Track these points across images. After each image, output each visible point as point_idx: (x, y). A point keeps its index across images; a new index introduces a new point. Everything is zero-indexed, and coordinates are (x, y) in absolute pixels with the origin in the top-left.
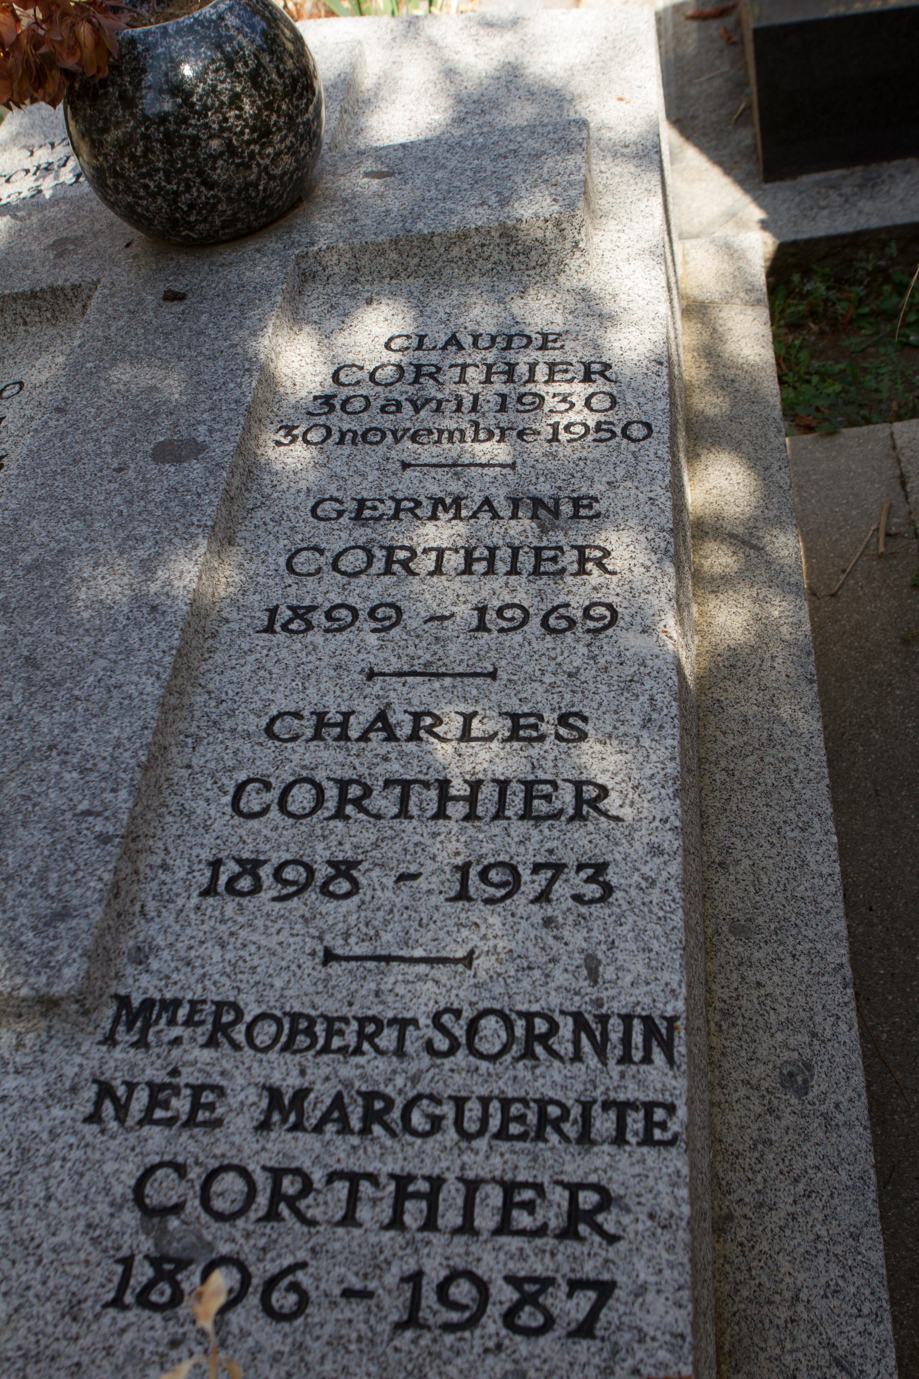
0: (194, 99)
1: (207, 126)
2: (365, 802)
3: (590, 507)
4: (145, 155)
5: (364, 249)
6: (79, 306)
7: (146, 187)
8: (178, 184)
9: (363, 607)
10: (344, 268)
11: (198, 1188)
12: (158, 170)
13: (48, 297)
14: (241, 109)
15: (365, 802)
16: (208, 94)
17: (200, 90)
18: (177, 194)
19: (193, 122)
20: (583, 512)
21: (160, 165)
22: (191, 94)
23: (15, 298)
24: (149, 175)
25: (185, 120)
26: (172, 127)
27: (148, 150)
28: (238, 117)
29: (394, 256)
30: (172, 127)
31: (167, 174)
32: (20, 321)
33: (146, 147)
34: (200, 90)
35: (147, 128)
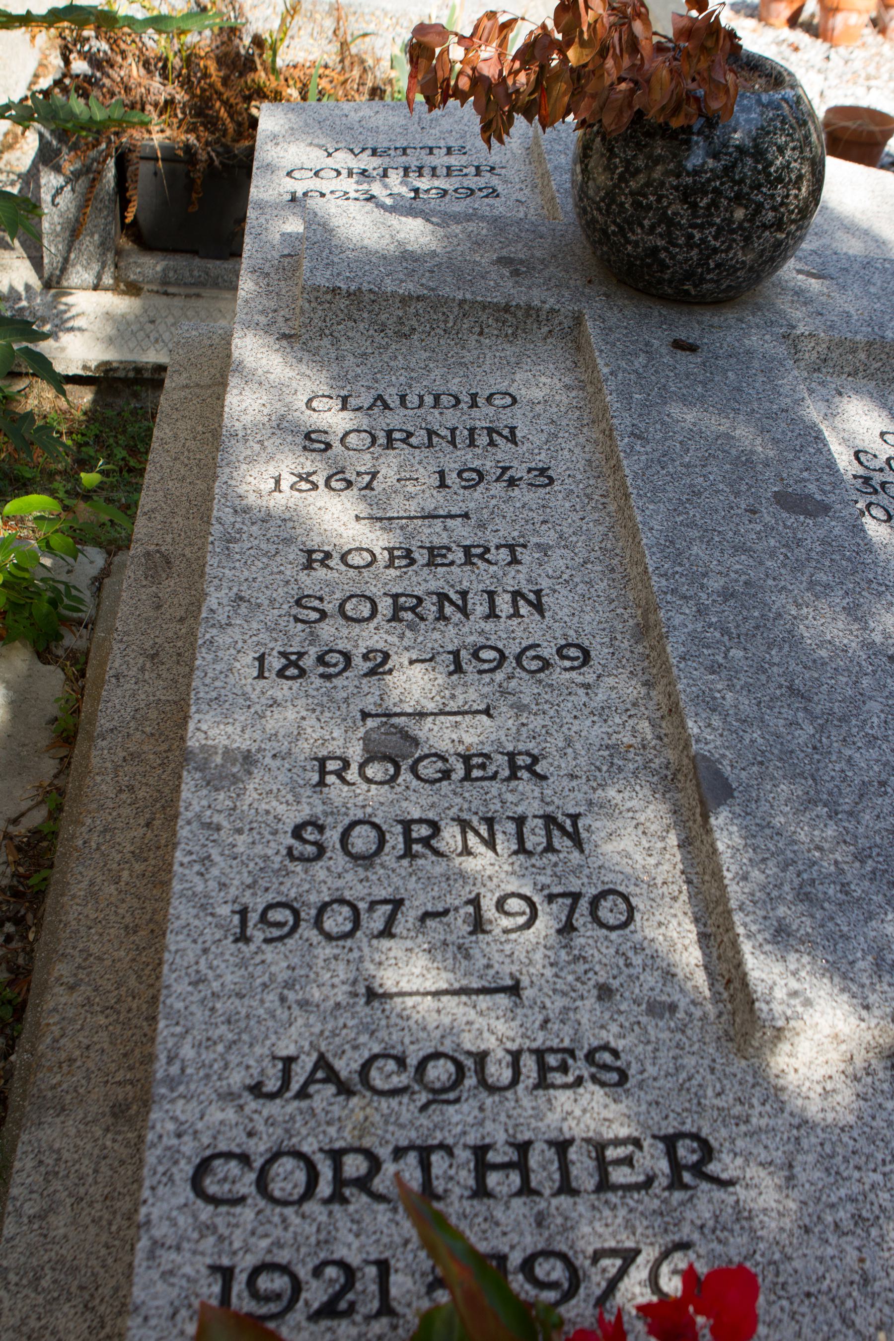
0: (772, 170)
1: (772, 197)
2: (433, 842)
3: (444, 556)
4: (708, 207)
5: (840, 343)
6: (545, 330)
7: (691, 237)
8: (723, 242)
9: (512, 650)
10: (815, 355)
11: (582, 1291)
12: (712, 225)
13: (520, 314)
14: (799, 190)
15: (433, 842)
16: (783, 168)
17: (778, 162)
18: (715, 251)
19: (764, 190)
20: (439, 560)
21: (718, 221)
22: (771, 164)
23: (484, 307)
24: (701, 227)
25: (759, 186)
26: (746, 190)
27: (714, 204)
28: (796, 196)
29: (862, 356)
30: (746, 190)
31: (720, 229)
32: (477, 330)
33: (713, 200)
34: (778, 162)
35: (722, 184)
